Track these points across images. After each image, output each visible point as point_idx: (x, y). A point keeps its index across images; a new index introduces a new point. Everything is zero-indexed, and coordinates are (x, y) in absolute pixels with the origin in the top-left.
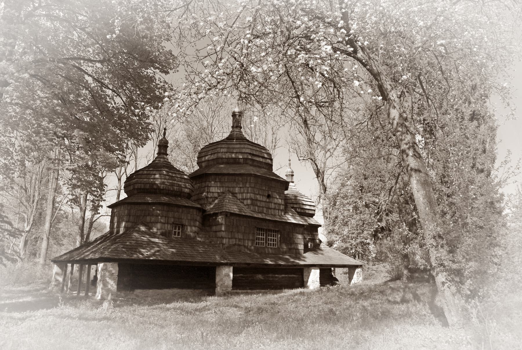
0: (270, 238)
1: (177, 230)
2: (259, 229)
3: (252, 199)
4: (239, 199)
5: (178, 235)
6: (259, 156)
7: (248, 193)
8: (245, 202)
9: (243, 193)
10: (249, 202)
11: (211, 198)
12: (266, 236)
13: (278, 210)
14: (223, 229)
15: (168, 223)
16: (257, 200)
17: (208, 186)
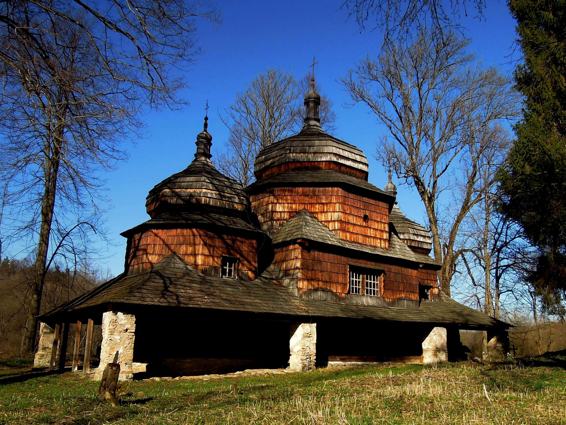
0: (369, 281)
1: (354, 286)
2: (355, 270)
3: (340, 221)
4: (321, 222)
6: (348, 159)
7: (334, 212)
8: (331, 226)
9: (327, 212)
10: (337, 225)
11: (278, 220)
13: (380, 239)
14: (298, 264)
16: (348, 223)
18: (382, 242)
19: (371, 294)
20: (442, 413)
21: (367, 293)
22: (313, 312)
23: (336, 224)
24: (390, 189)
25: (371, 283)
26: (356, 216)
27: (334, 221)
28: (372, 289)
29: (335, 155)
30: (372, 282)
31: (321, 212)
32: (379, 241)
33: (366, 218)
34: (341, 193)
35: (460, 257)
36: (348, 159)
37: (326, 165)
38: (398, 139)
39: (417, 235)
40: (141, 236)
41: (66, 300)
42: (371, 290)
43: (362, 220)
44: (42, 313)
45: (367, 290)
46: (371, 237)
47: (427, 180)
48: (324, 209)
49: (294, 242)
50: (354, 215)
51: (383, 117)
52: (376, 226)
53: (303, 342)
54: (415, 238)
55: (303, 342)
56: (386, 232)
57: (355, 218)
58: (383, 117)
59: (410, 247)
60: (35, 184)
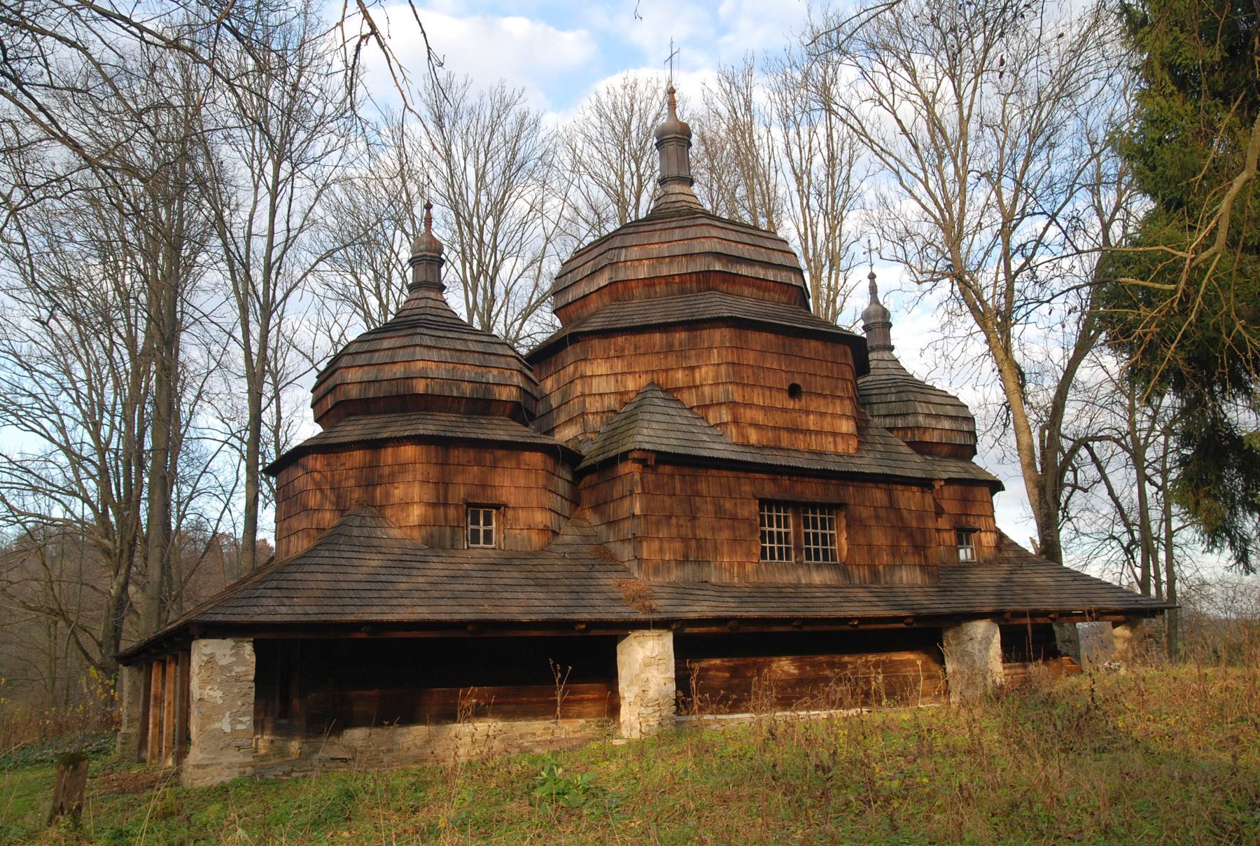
3: (732, 404)
4: (692, 408)
6: (750, 262)
12: (797, 527)
15: (446, 505)
17: (582, 377)
18: (839, 440)
19: (817, 558)
20: (85, 722)
21: (809, 558)
22: (664, 606)
24: (876, 316)
27: (720, 404)
29: (718, 255)
30: (819, 531)
31: (689, 388)
32: (831, 439)
33: (794, 391)
34: (731, 341)
35: (1083, 452)
36: (750, 262)
37: (698, 282)
39: (937, 416)
40: (91, 505)
42: (772, 549)
43: (786, 395)
44: (124, 646)
45: (808, 550)
46: (810, 431)
47: (989, 277)
49: (624, 456)
50: (763, 387)
52: (645, 431)
53: (646, 663)
55: (646, 663)
56: (848, 417)
57: (767, 393)
59: (911, 444)
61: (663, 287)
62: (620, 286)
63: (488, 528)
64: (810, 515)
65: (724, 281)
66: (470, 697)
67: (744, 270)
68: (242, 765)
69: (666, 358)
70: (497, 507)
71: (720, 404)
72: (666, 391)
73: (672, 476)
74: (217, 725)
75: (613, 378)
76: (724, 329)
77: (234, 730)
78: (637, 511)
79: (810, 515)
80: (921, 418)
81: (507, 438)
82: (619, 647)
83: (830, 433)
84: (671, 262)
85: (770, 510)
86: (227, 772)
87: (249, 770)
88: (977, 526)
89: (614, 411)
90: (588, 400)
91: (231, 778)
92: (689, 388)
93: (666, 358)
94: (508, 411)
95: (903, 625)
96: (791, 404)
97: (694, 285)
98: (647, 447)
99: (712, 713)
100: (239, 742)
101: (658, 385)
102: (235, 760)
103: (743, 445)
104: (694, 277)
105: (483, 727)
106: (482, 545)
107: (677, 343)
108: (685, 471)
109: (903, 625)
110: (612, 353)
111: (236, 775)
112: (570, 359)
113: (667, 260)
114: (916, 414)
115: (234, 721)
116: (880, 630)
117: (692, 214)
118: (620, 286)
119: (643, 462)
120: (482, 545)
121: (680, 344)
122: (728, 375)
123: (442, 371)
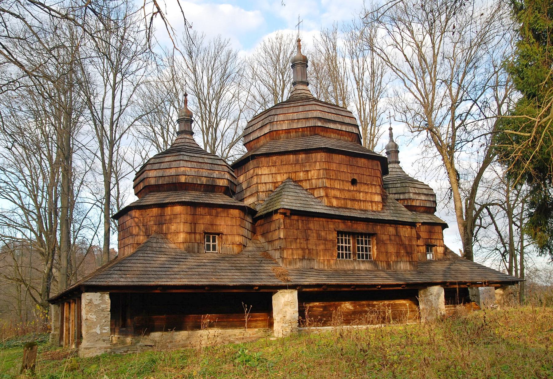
0: (360, 245)
1: (211, 244)
5: (350, 258)
6: (335, 122)
15: (195, 233)
17: (257, 175)
18: (374, 204)
19: (363, 258)
20: (35, 329)
21: (359, 258)
22: (294, 279)
23: (321, 191)
24: (392, 147)
25: (362, 247)
26: (343, 181)
27: (320, 188)
28: (364, 253)
29: (320, 119)
30: (364, 246)
32: (370, 204)
34: (325, 159)
36: (335, 122)
37: (310, 131)
38: (412, 92)
39: (419, 194)
41: (42, 275)
43: (350, 184)
47: (444, 130)
48: (308, 177)
50: (339, 180)
51: (395, 69)
53: (285, 304)
54: (417, 197)
55: (285, 304)
57: (341, 183)
58: (395, 69)
59: (406, 207)
60: (477, 105)
61: (294, 133)
62: (274, 133)
63: (214, 243)
64: (360, 239)
65: (322, 131)
66: (207, 319)
67: (332, 126)
68: (106, 348)
69: (295, 166)
70: (218, 234)
71: (320, 188)
72: (295, 182)
73: (298, 220)
74: (94, 330)
75: (271, 176)
76: (322, 153)
77: (101, 333)
78: (282, 236)
79: (360, 239)
80: (411, 195)
81: (223, 203)
82: (273, 297)
83: (369, 201)
84: (298, 122)
85: (342, 236)
86: (99, 351)
87: (109, 350)
88: (435, 244)
89: (272, 191)
90: (259, 185)
91: (101, 354)
92: (306, 180)
93: (295, 166)
94: (223, 191)
95: (401, 288)
96: (352, 188)
97: (309, 133)
98: (286, 207)
99: (314, 326)
100: (104, 338)
101: (292, 179)
102: (102, 346)
103: (330, 207)
104: (309, 129)
105: (213, 331)
106: (211, 251)
107: (300, 159)
108: (304, 218)
109: (401, 288)
110: (271, 164)
111: (103, 352)
112: (251, 167)
113: (296, 121)
114: (409, 193)
115: (101, 329)
116: (387, 290)
117: (308, 99)
118: (274, 133)
119: (284, 214)
120: (211, 251)
121: (302, 160)
122: (324, 174)
123: (193, 172)
